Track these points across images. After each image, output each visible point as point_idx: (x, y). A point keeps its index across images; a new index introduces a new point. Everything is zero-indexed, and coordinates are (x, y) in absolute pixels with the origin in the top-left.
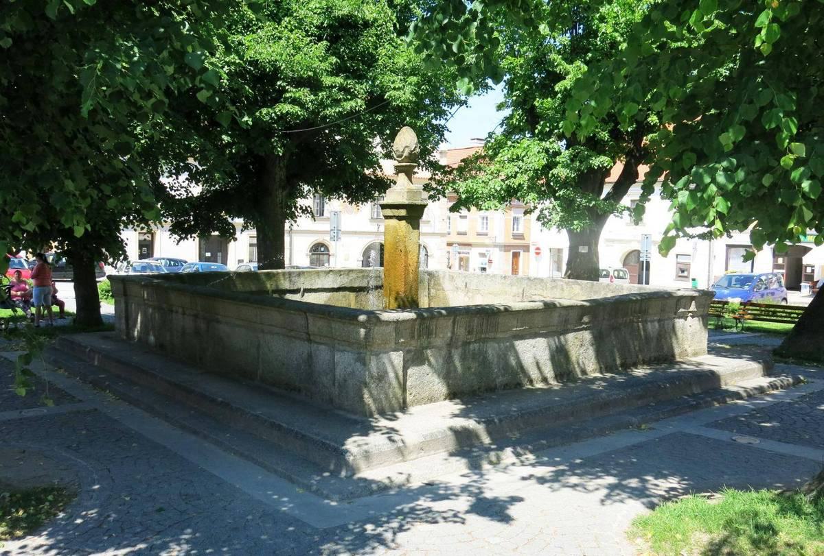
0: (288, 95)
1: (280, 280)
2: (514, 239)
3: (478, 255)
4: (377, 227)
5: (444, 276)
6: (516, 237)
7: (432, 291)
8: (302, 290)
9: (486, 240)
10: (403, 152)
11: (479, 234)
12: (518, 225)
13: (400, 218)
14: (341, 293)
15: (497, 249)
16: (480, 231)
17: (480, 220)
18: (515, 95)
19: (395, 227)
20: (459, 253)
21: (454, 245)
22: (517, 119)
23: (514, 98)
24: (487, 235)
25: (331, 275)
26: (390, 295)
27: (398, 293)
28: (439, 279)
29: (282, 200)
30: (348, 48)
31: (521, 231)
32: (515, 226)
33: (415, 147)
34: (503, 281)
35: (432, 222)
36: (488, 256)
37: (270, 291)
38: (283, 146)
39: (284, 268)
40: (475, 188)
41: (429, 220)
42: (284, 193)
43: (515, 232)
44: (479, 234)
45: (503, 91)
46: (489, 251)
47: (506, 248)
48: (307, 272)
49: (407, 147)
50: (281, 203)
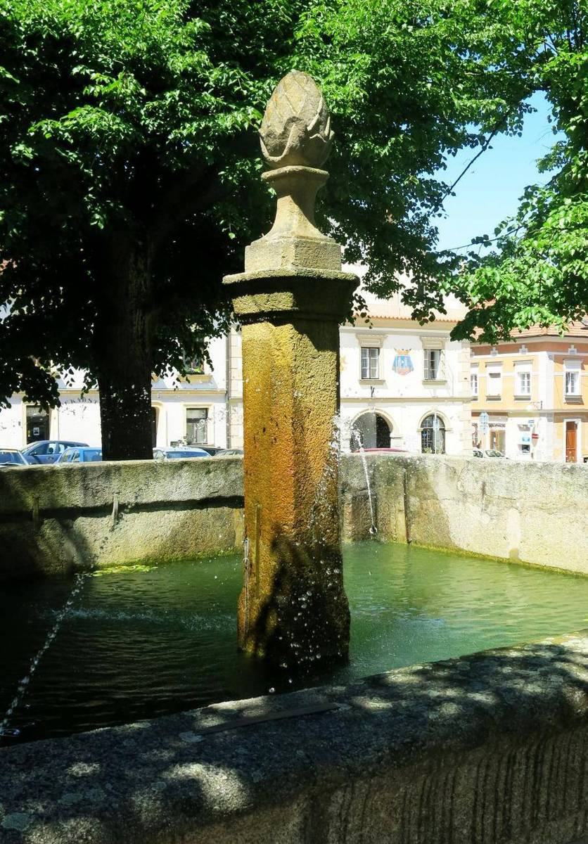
0: (90, 90)
1: (59, 487)
2: (568, 403)
3: (489, 376)
4: (370, 391)
5: (436, 471)
6: (571, 400)
7: (413, 500)
8: (115, 506)
9: (528, 407)
10: (284, 134)
11: (517, 399)
12: (573, 384)
13: (277, 318)
14: (212, 511)
15: (544, 419)
16: (519, 393)
17: (519, 380)
18: (574, 123)
19: (266, 344)
20: (491, 426)
21: (482, 414)
22: (579, 168)
23: (573, 128)
24: (529, 399)
25: (185, 474)
26: (259, 531)
27: (278, 529)
28: (425, 474)
29: (143, 331)
30: (235, 14)
31: (577, 393)
32: (570, 386)
33: (319, 123)
34: (567, 478)
35: (450, 383)
36: (532, 428)
37: (35, 512)
38: (106, 211)
39: (152, 458)
40: (498, 279)
41: (444, 379)
42: (148, 318)
43: (570, 393)
44: (517, 399)
45: (550, 121)
46: (533, 421)
47: (557, 416)
48: (126, 467)
49: (293, 120)
50: (142, 336)
